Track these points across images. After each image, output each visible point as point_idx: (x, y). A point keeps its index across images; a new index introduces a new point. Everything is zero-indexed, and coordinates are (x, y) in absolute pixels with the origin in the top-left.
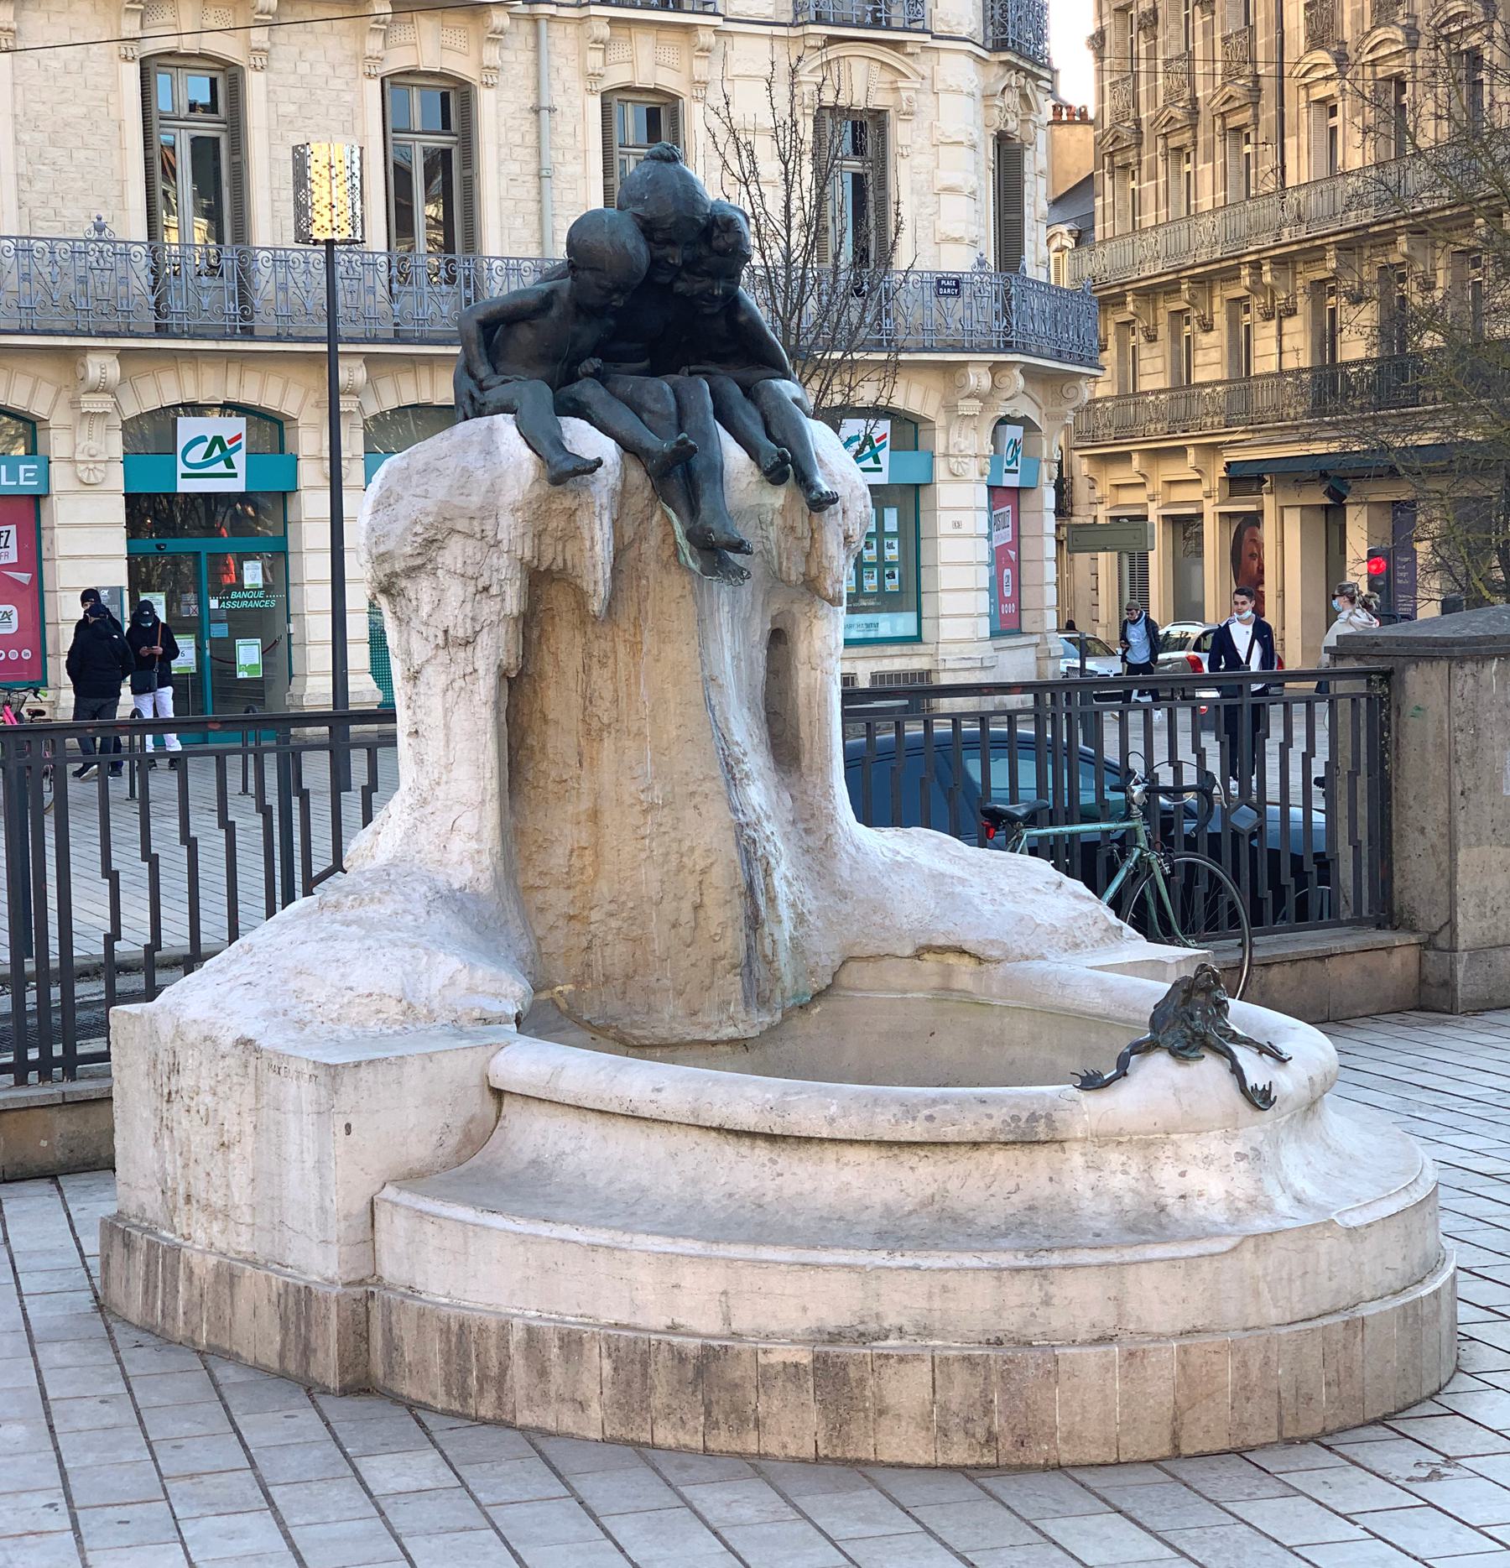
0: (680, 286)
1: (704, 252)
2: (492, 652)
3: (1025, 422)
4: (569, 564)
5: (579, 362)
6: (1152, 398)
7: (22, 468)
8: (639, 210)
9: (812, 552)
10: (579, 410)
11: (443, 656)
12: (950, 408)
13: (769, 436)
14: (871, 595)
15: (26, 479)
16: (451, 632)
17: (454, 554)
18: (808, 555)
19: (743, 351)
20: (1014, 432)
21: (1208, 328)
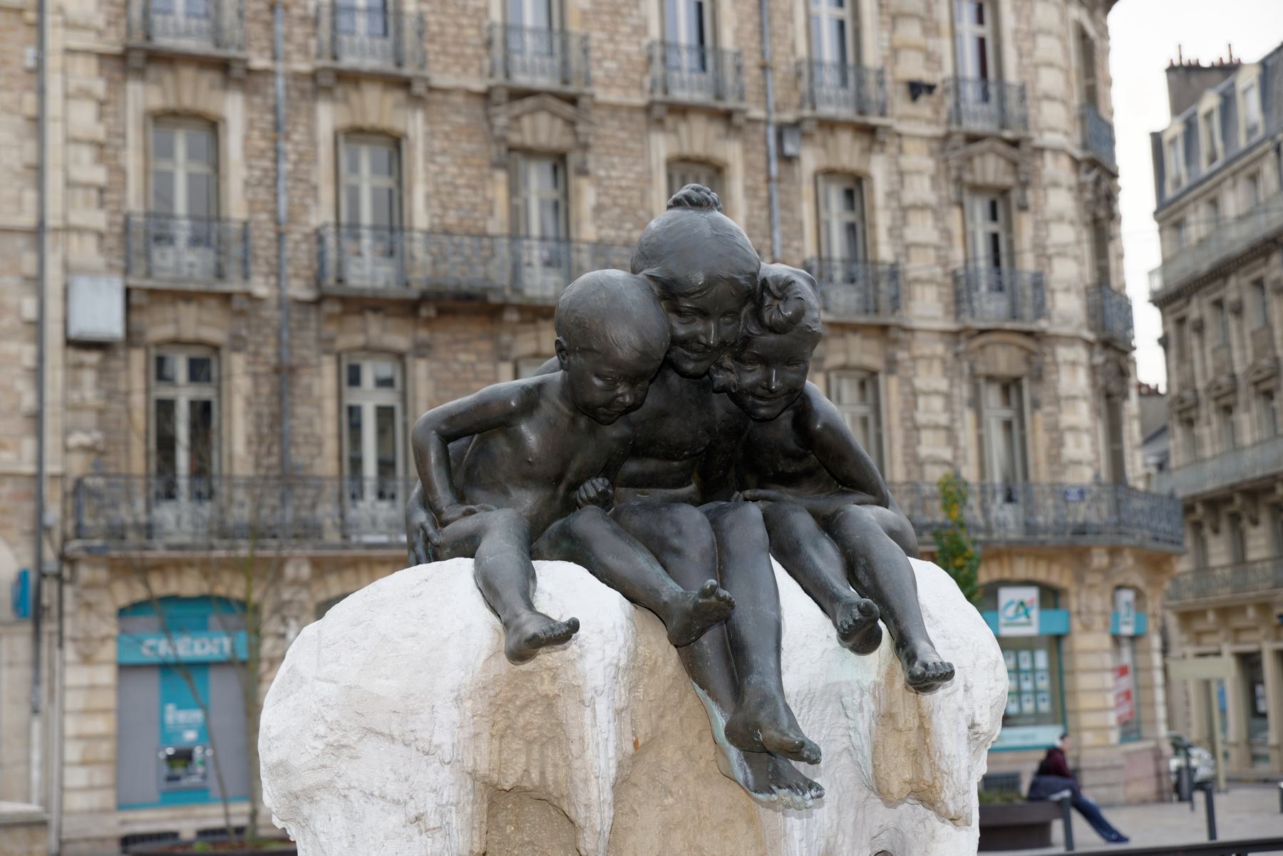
1: (754, 330)
5: (574, 486)
8: (653, 271)
9: (922, 743)
10: (577, 552)
12: (1079, 579)
13: (852, 579)
14: (1028, 716)
21: (1255, 522)
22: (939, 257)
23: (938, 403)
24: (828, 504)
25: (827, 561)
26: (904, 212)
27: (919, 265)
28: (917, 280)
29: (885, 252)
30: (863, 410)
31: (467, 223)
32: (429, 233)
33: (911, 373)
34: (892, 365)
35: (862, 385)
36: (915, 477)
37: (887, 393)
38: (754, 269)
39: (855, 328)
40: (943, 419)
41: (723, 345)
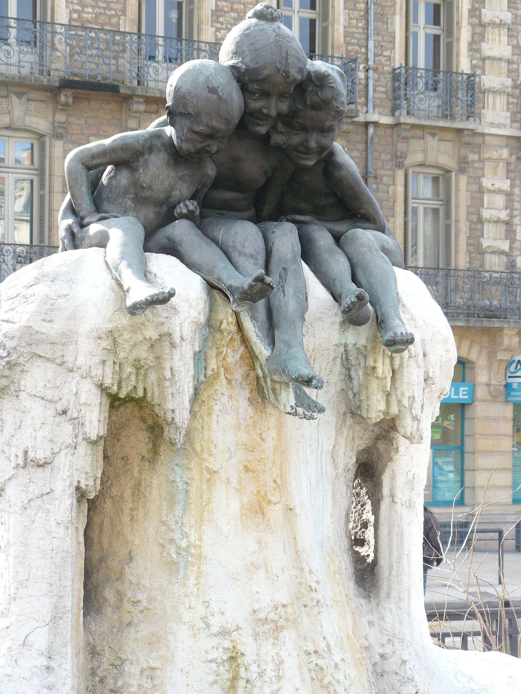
0: (278, 139)
4: (149, 395)
7: (461, 389)
10: (172, 249)
11: (23, 476)
13: (354, 279)
15: (463, 395)
16: (30, 453)
18: (388, 395)
19: (342, 205)
22: (509, 71)
23: (500, 200)
24: (339, 227)
25: (339, 265)
26: (480, 29)
27: (492, 79)
28: (489, 91)
29: (464, 65)
30: (435, 204)
31: (102, 19)
32: (69, 27)
33: (479, 172)
34: (464, 165)
35: (436, 179)
36: (476, 264)
37: (457, 190)
38: (301, 66)
39: (434, 131)
40: (504, 215)
41: (279, 115)
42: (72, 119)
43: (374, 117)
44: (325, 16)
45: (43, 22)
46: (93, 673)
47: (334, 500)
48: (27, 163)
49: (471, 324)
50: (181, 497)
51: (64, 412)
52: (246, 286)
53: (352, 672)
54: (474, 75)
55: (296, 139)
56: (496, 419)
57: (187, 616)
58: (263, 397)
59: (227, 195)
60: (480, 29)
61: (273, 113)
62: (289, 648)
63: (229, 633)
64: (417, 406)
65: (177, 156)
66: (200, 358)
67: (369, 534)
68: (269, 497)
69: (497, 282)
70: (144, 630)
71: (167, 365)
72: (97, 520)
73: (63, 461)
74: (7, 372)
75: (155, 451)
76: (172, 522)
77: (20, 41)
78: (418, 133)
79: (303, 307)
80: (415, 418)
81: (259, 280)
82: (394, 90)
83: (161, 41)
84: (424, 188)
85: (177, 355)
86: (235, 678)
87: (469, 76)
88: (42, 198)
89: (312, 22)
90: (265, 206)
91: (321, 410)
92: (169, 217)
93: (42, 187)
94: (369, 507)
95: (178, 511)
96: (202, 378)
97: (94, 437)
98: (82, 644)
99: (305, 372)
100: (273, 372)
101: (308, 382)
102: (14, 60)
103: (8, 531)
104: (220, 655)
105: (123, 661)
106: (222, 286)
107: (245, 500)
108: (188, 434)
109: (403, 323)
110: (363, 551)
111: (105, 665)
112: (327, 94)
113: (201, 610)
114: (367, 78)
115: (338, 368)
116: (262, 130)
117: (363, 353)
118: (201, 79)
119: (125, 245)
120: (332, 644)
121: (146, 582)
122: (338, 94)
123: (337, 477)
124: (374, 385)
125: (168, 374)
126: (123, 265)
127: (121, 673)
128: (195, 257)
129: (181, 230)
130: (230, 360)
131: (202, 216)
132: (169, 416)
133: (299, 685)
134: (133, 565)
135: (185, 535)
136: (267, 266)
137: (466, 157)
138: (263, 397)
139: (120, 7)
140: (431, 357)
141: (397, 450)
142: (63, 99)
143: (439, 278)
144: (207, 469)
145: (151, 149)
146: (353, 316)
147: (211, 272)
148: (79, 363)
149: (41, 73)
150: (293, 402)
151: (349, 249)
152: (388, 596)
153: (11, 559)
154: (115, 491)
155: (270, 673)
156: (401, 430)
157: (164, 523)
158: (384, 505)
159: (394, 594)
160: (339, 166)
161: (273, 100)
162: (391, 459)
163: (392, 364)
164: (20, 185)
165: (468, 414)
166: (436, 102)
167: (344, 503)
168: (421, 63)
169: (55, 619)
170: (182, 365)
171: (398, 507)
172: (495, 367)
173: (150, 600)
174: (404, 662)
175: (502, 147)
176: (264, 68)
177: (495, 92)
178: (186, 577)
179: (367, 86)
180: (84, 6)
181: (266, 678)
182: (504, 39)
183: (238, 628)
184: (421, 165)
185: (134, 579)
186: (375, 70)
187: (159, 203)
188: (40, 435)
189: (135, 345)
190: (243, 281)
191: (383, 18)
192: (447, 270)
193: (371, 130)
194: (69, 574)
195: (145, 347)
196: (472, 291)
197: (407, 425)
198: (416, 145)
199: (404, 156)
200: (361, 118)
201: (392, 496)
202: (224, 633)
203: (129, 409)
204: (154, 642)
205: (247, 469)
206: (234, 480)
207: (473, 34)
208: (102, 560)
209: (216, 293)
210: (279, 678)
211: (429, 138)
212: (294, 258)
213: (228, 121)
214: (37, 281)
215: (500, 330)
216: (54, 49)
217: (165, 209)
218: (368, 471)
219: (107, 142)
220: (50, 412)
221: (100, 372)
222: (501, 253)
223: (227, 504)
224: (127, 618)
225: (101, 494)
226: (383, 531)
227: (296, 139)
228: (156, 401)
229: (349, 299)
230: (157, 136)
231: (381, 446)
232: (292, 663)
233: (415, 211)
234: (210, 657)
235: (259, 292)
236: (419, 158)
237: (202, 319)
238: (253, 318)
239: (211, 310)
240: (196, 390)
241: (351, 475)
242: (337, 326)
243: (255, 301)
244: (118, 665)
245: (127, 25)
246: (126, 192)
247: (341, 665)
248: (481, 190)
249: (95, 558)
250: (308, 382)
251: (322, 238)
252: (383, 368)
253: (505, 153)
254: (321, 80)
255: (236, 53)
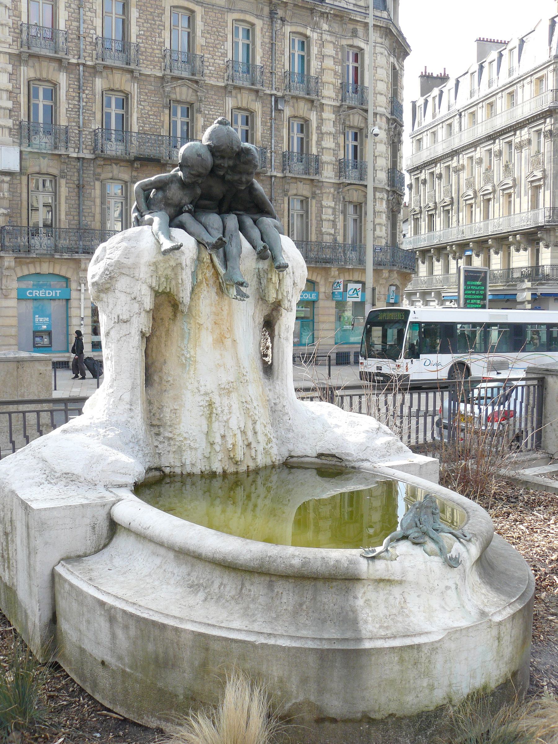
0: (228, 177)
2: (141, 323)
3: (396, 285)
6: (521, 259)
10: (181, 226)
13: (262, 239)
17: (122, 283)
18: (277, 291)
19: (258, 208)
20: (393, 288)
23: (330, 211)
24: (256, 217)
25: (255, 233)
27: (327, 157)
28: (325, 162)
29: (314, 151)
33: (321, 199)
35: (302, 201)
36: (320, 239)
39: (301, 180)
40: (332, 218)
41: (229, 167)
42: (140, 174)
43: (274, 174)
44: (252, 128)
45: (127, 131)
46: (150, 412)
47: (254, 337)
48: (120, 194)
49: (318, 266)
50: (187, 335)
51: (135, 298)
52: (214, 242)
53: (262, 411)
54: (318, 155)
55: (236, 177)
56: (328, 308)
57: (190, 387)
58: (222, 292)
59: (207, 202)
60: (321, 135)
61: (226, 165)
62: (234, 401)
63: (209, 394)
64: (290, 295)
65: (184, 185)
66: (194, 274)
67: (269, 352)
68: (225, 335)
69: (329, 247)
70: (171, 393)
71: (180, 277)
72: (150, 346)
73: (135, 320)
74: (109, 281)
75: (175, 315)
76: (183, 347)
77: (117, 140)
78: (294, 181)
79: (240, 252)
80: (289, 301)
81: (220, 239)
82: (283, 162)
83: (179, 139)
84: (297, 205)
85: (184, 273)
86: (211, 413)
87: (316, 156)
88: (126, 210)
89: (247, 131)
90: (223, 208)
91: (248, 297)
92: (180, 212)
93: (126, 205)
94: (269, 340)
95: (186, 342)
96: (195, 283)
97: (148, 309)
98: (145, 399)
99: (241, 280)
100: (226, 280)
101: (242, 284)
102: (114, 149)
103: (111, 351)
104: (204, 403)
105: (163, 406)
106: (204, 242)
107: (215, 337)
108: (189, 308)
109: (283, 259)
110: (267, 359)
111: (155, 408)
112: (250, 157)
113: (196, 384)
114: (271, 156)
115: (255, 279)
116: (221, 173)
117: (266, 272)
118: (194, 150)
119: (160, 224)
120: (253, 398)
121: (172, 373)
122: (255, 157)
123: (255, 327)
124: (271, 286)
125: (180, 281)
126: (160, 233)
127: (162, 412)
128: (192, 230)
129: (185, 217)
130: (207, 275)
131: (195, 212)
132: (181, 300)
133: (239, 416)
134: (166, 365)
135: (189, 352)
136: (224, 233)
137: (315, 192)
138: (222, 292)
139: (161, 124)
140: (296, 274)
141: (281, 315)
142: (136, 165)
143: (302, 244)
144: (198, 323)
145: (172, 182)
146: (262, 256)
147: (199, 236)
148: (141, 277)
149: (126, 154)
150: (235, 293)
151: (260, 226)
152: (277, 378)
153: (113, 363)
154: (158, 333)
155: (226, 411)
156: (283, 306)
157: (179, 347)
158: (276, 339)
159: (280, 377)
160: (256, 190)
161: (226, 160)
162: (278, 319)
163: (279, 277)
164: (117, 205)
165: (316, 305)
166: (302, 167)
167: (258, 338)
168: (295, 150)
169: (133, 388)
170: (186, 277)
171: (282, 340)
172: (328, 285)
173: (174, 380)
174: (284, 406)
175: (331, 187)
176: (222, 145)
177: (328, 163)
178: (189, 370)
179: (271, 160)
180: (145, 124)
181: (224, 413)
182: (332, 140)
183: (212, 392)
184: (296, 195)
185: (167, 371)
186: (275, 153)
187: (176, 206)
188: (124, 308)
189: (166, 269)
190: (213, 240)
191: (278, 130)
192: (307, 242)
193: (273, 179)
194: (139, 369)
195: (170, 269)
196: (318, 251)
197: (286, 304)
198: (293, 186)
199: (288, 191)
200: (269, 174)
201: (279, 335)
202: (206, 394)
203: (163, 297)
204: (176, 398)
205: (215, 323)
206: (210, 328)
207: (318, 137)
208: (152, 363)
209: (202, 247)
210: (230, 413)
211: (299, 183)
212: (236, 230)
213: (206, 169)
214: (122, 240)
215: (330, 268)
216: (132, 143)
217: (178, 209)
218: (269, 325)
219: (153, 178)
220: (129, 299)
221: (150, 281)
222: (331, 234)
223: (207, 339)
224: (164, 388)
225: (152, 335)
226: (275, 350)
227: (236, 177)
228: (175, 293)
229: (260, 248)
230: (175, 176)
231: (274, 313)
232: (235, 406)
233: (293, 215)
234: (200, 404)
235: (220, 245)
236: (294, 192)
237: (195, 257)
238: (217, 256)
239: (199, 253)
240: (193, 288)
241: (261, 326)
242: (255, 260)
243: (218, 249)
244: (161, 408)
245: (164, 132)
246: (161, 201)
247: (257, 407)
248: (322, 206)
249: (150, 362)
250: (242, 284)
251: (248, 221)
252: (275, 279)
253: (332, 190)
254: (247, 151)
255: (210, 139)
